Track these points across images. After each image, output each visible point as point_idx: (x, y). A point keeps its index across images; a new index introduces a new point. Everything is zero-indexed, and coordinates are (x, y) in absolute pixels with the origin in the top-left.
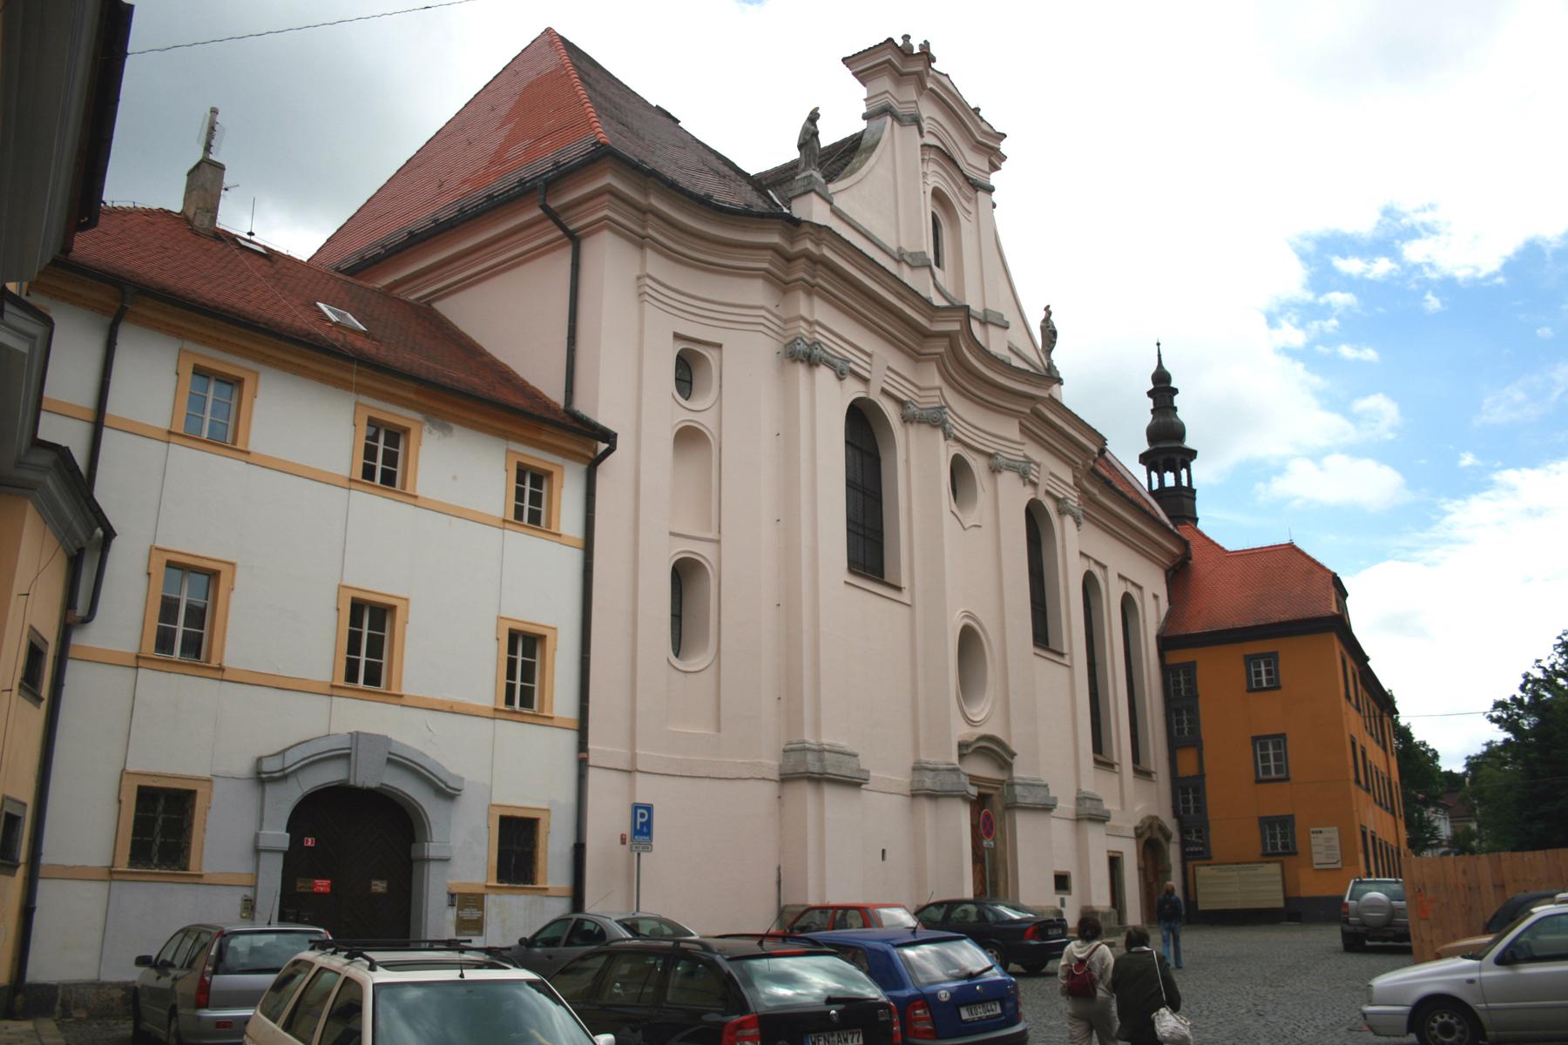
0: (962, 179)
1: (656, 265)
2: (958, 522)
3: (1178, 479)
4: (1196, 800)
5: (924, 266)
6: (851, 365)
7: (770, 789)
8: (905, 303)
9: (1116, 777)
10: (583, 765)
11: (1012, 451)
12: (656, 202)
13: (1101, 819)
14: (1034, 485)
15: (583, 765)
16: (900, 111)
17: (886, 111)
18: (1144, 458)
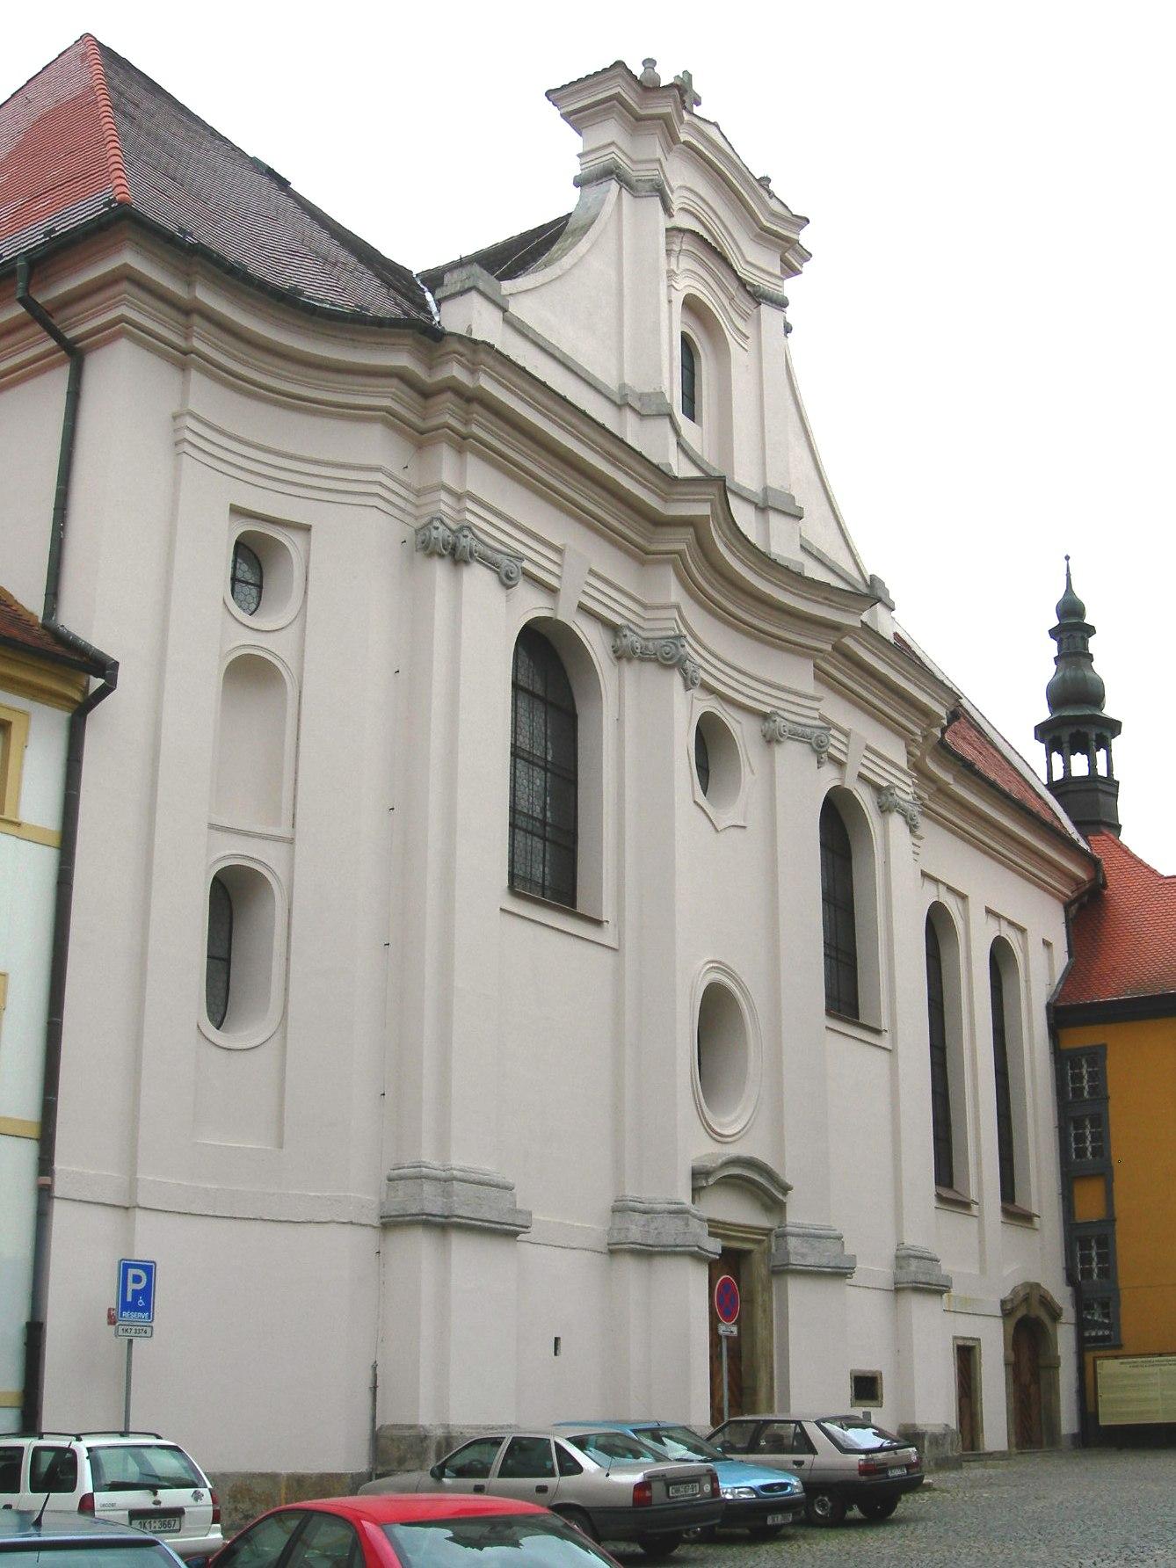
0: (736, 284)
1: (204, 395)
2: (705, 817)
3: (1092, 765)
4: (1103, 1258)
5: (659, 415)
6: (526, 564)
7: (368, 1238)
8: (619, 469)
9: (972, 1224)
10: (45, 1195)
11: (794, 708)
12: (206, 296)
13: (937, 1290)
14: (840, 764)
15: (45, 1195)
16: (634, 174)
17: (610, 173)
18: (1042, 732)
